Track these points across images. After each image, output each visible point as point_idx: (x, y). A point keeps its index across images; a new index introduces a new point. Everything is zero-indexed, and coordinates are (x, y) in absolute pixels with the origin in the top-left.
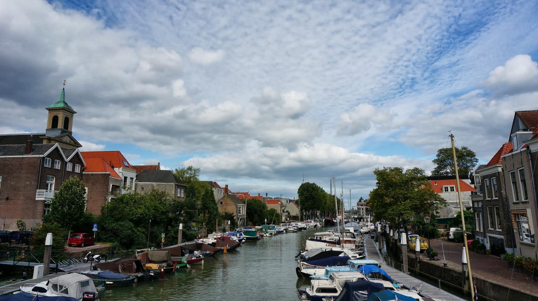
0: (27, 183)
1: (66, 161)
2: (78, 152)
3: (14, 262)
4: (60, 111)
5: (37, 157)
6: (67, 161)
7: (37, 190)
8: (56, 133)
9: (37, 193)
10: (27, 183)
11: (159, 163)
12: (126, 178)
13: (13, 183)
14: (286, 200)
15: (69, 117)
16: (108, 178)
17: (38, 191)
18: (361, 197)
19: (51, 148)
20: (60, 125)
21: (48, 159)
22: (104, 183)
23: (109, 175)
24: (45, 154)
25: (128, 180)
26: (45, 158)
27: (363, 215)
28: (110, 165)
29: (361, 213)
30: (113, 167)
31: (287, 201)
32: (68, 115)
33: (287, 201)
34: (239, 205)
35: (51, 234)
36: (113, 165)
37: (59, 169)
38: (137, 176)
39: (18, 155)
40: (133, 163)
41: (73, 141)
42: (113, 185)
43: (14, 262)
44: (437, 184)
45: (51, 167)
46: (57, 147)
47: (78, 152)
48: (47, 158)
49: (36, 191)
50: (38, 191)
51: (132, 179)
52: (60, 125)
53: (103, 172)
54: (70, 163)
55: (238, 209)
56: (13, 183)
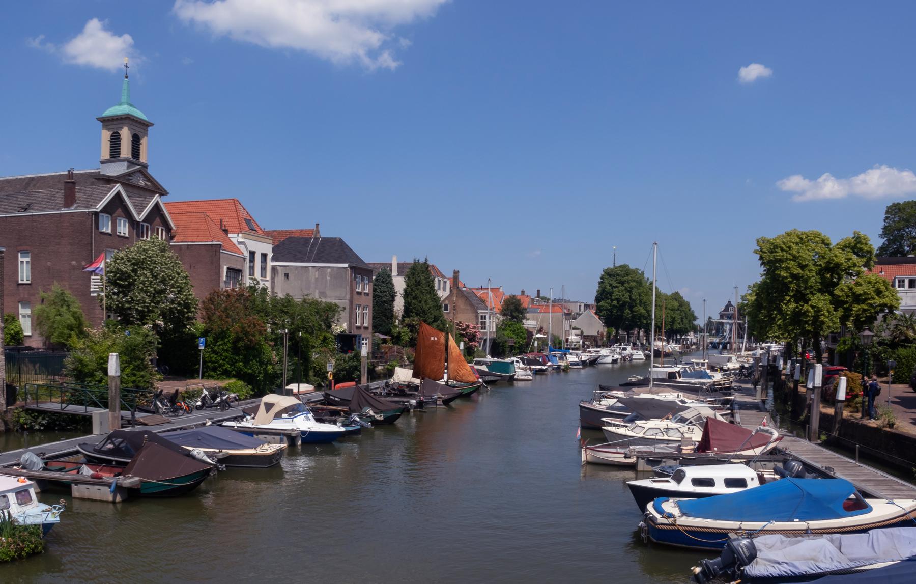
0: (74, 263)
1: (138, 220)
2: (158, 201)
3: (61, 406)
4: (123, 121)
5: (85, 212)
6: (140, 219)
7: (93, 277)
8: (116, 170)
9: (92, 284)
10: (74, 263)
11: (317, 225)
12: (252, 254)
13: (49, 264)
14: (579, 304)
15: (140, 135)
16: (217, 254)
17: (93, 279)
18: (729, 302)
19: (107, 194)
20: (126, 150)
21: (145, 224)
22: (212, 263)
23: (220, 248)
24: (97, 207)
25: (258, 258)
26: (100, 214)
27: (730, 337)
28: (221, 227)
29: (728, 331)
30: (226, 232)
31: (580, 306)
32: (139, 131)
33: (580, 306)
34: (482, 313)
35: (116, 355)
36: (227, 228)
37: (127, 235)
38: (274, 250)
39: (52, 209)
40: (266, 223)
41: (151, 182)
42: (228, 269)
43: (61, 406)
44: (883, 273)
45: (112, 231)
46: (119, 191)
47: (158, 201)
48: (143, 223)
49: (90, 282)
50: (93, 279)
51: (264, 256)
52: (126, 150)
53: (208, 242)
54: (105, 215)
55: (480, 320)
56: (49, 264)
